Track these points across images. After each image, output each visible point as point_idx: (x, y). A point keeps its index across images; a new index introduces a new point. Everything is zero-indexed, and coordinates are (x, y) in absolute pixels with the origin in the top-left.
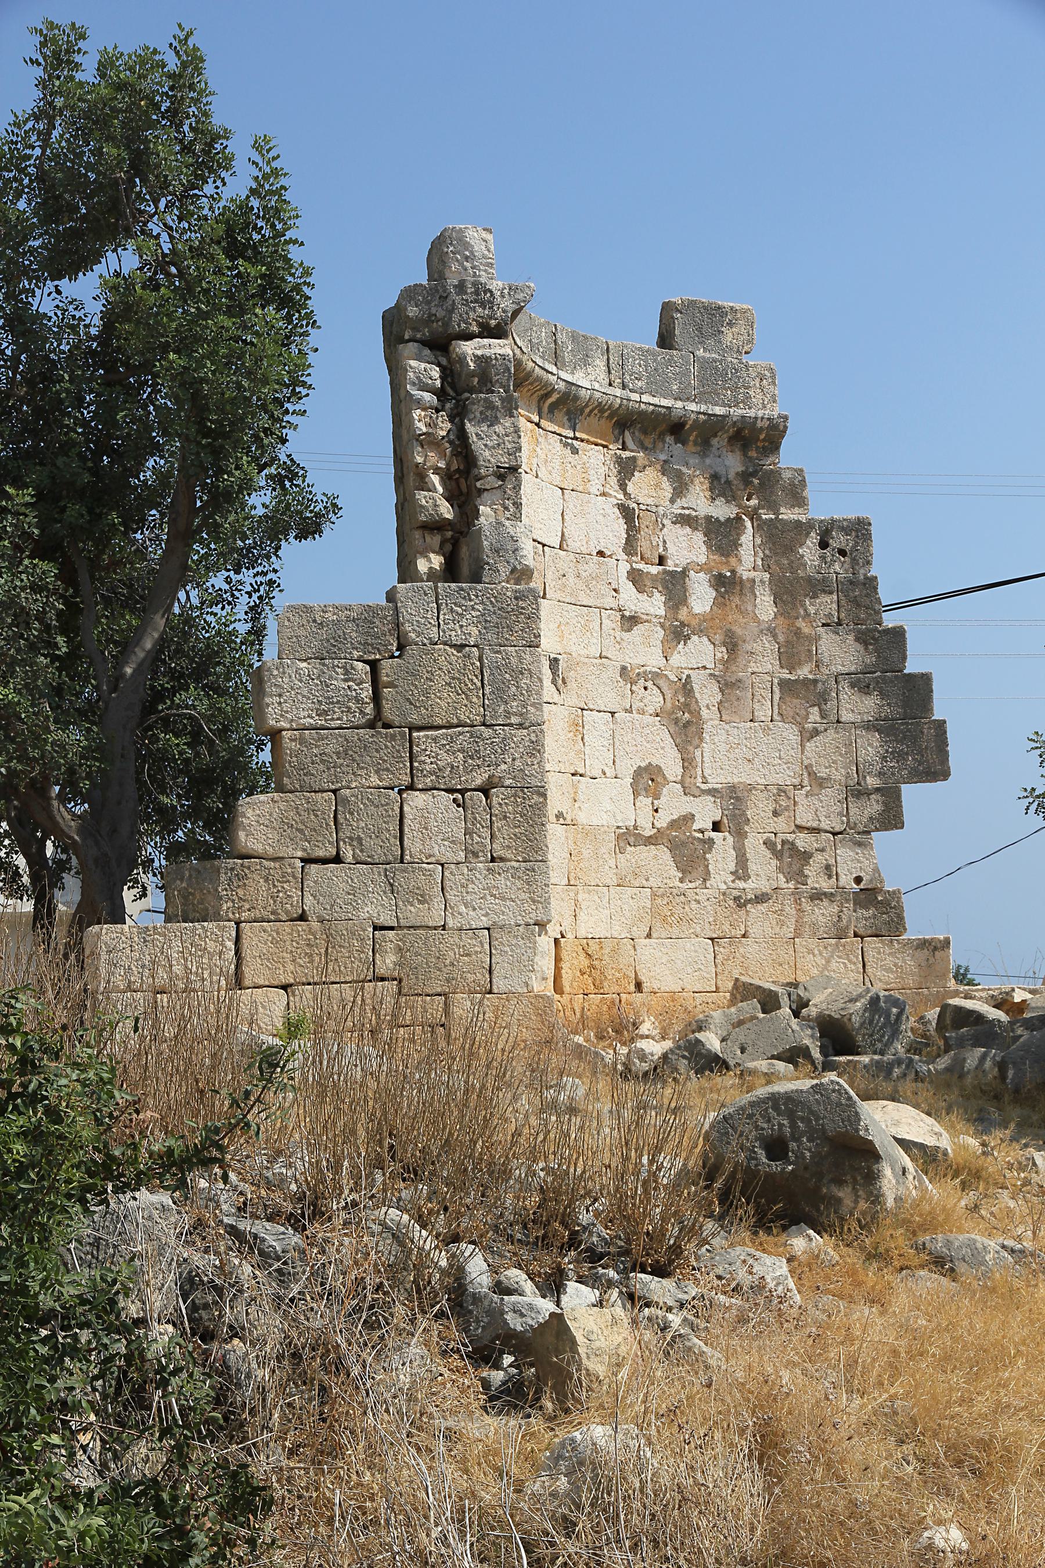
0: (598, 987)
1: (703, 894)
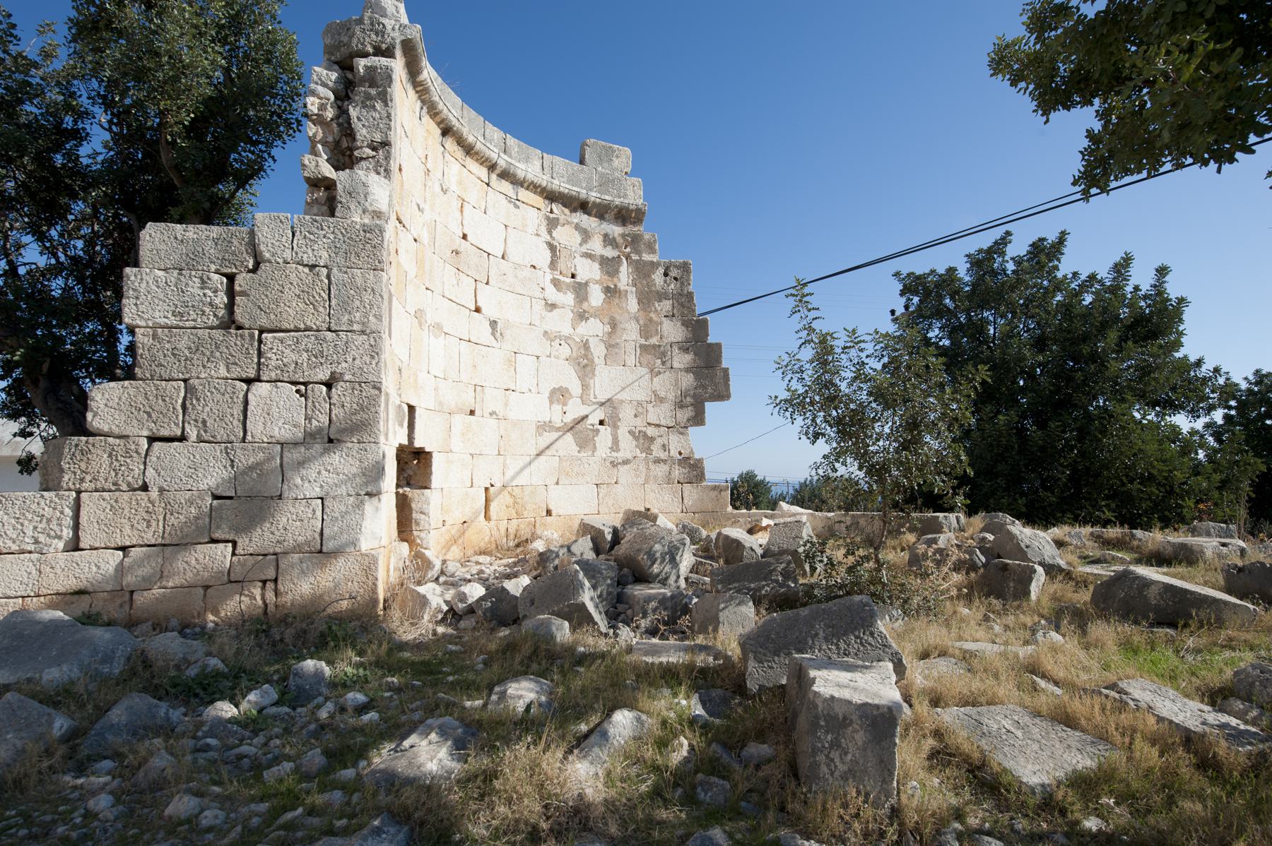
0: (519, 516)
1: (592, 460)
